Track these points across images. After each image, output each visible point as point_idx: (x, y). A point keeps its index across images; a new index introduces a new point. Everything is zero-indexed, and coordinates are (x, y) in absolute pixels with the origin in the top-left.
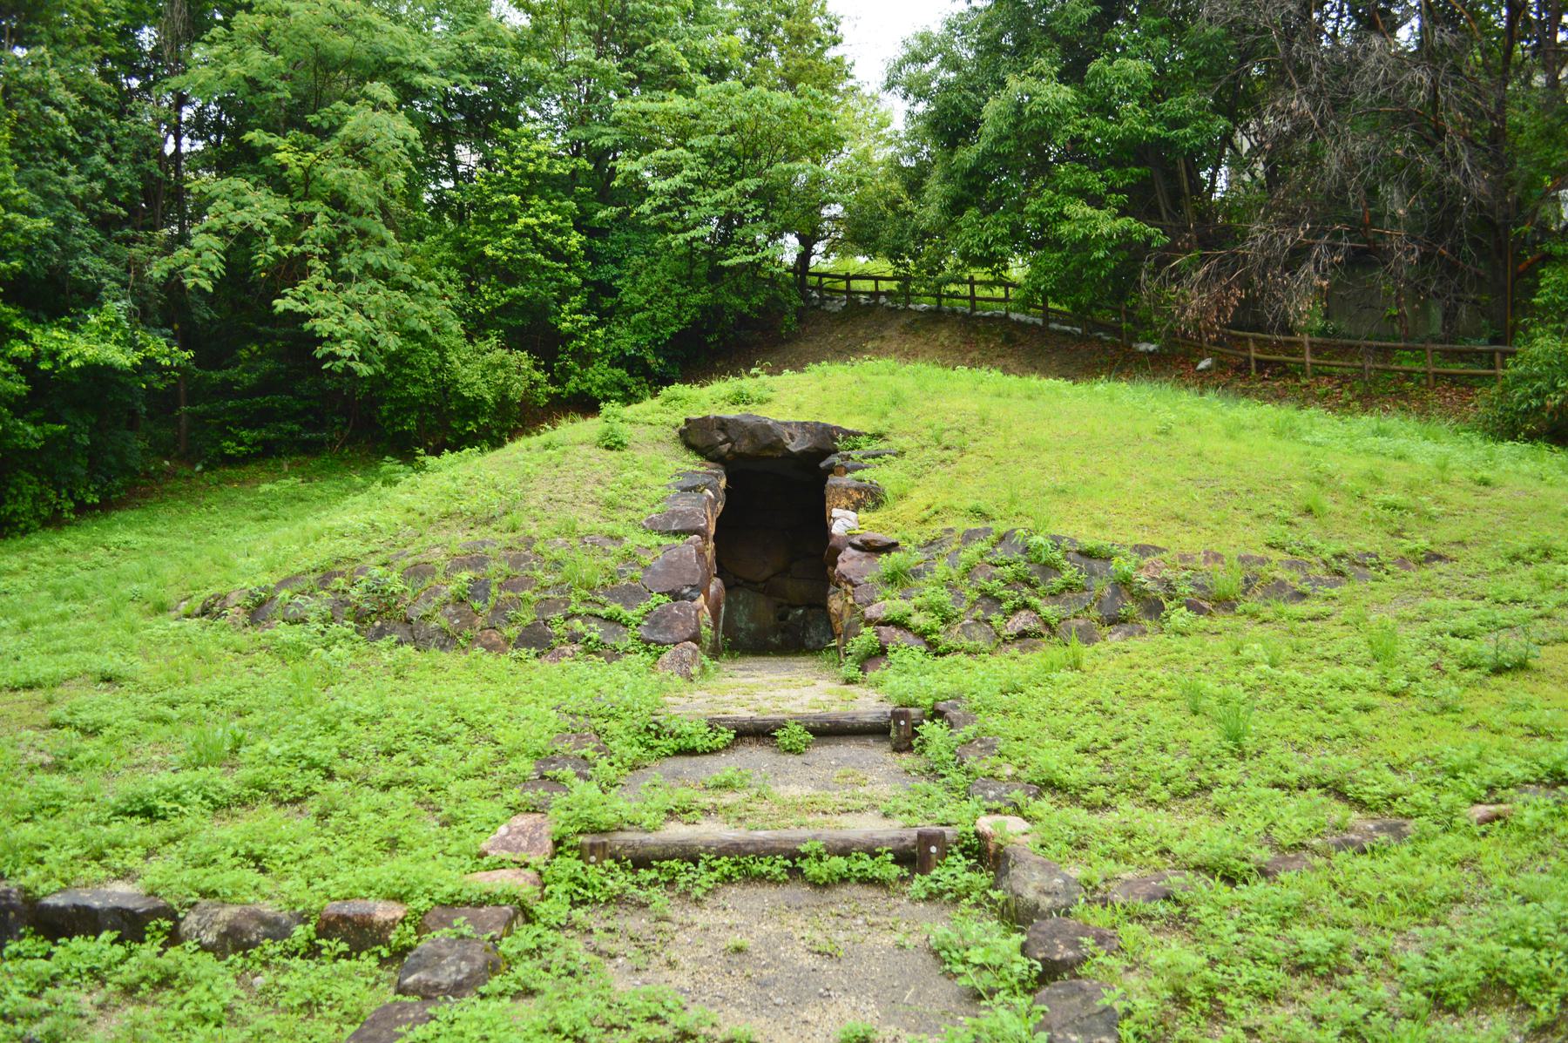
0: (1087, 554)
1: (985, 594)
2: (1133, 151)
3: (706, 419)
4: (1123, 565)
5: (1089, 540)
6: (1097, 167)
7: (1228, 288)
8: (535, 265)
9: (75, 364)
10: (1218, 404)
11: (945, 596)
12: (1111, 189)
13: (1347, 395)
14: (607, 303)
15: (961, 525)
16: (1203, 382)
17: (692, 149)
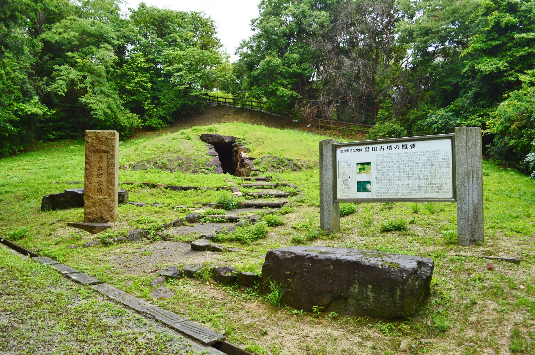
0: (289, 160)
1: (273, 166)
2: (294, 75)
3: (207, 134)
4: (295, 162)
5: (290, 158)
6: (285, 78)
7: (315, 109)
8: (140, 91)
9: (29, 113)
10: (311, 135)
11: (266, 166)
12: (289, 84)
13: (340, 134)
14: (156, 102)
15: (267, 155)
16: (309, 130)
17: (184, 64)
